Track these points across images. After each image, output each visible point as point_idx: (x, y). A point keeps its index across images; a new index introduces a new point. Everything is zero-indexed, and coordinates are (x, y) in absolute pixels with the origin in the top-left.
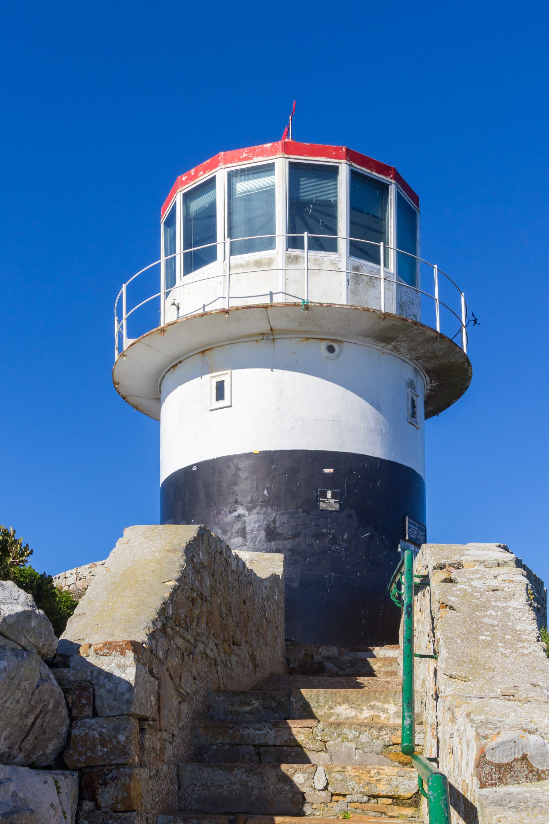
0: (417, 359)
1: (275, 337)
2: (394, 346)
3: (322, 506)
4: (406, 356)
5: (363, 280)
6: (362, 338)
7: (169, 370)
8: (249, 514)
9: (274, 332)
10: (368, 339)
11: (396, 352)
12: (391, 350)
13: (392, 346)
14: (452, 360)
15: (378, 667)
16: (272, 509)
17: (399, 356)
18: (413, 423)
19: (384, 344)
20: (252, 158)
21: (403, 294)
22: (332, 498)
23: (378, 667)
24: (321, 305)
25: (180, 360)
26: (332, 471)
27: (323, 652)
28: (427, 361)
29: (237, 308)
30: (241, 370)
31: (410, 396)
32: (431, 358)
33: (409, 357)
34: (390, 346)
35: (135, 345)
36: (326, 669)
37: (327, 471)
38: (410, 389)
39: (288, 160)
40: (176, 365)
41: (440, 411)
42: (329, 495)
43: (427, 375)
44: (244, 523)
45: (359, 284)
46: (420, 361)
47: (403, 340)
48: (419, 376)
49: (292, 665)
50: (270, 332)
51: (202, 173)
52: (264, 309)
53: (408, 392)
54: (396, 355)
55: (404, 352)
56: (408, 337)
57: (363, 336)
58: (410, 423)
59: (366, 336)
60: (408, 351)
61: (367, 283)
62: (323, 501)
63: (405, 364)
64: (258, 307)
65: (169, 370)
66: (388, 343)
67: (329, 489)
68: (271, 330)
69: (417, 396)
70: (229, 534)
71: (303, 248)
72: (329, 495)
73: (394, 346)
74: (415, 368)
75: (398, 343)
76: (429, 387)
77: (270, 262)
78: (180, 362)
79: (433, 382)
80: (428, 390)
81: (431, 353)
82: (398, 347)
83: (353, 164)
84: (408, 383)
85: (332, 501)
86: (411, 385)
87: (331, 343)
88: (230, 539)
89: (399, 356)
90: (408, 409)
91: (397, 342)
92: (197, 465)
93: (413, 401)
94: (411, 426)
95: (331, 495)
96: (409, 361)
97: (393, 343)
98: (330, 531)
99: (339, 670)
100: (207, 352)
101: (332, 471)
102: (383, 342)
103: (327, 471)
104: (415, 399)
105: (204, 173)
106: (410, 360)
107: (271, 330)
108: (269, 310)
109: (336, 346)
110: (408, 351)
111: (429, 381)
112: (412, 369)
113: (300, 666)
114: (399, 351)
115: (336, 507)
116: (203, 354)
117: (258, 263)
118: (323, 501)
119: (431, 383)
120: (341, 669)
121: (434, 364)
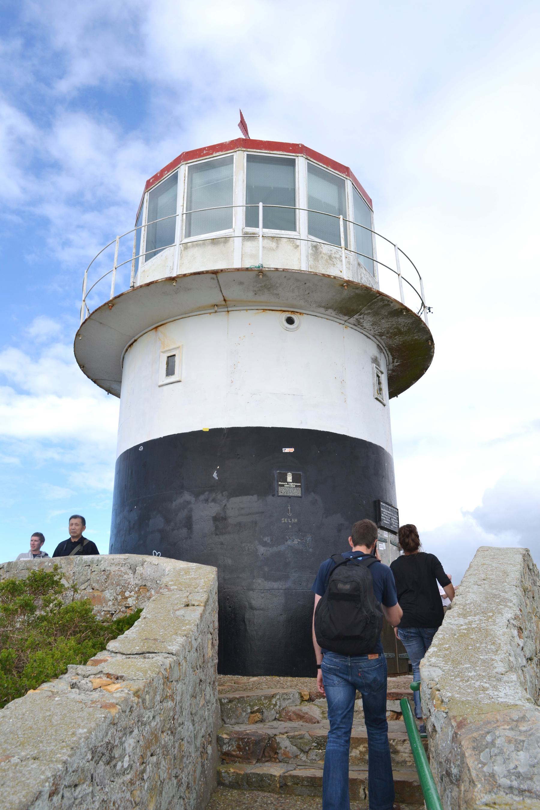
0: (381, 335)
1: (230, 309)
2: (357, 319)
3: (282, 491)
4: (370, 332)
5: (322, 257)
6: (322, 310)
7: (127, 350)
8: (196, 500)
9: (228, 302)
10: (330, 311)
11: (359, 326)
12: (354, 325)
13: (355, 319)
14: (416, 337)
15: (361, 752)
16: (223, 495)
17: (362, 331)
18: (380, 399)
19: (346, 318)
20: (212, 154)
21: (363, 275)
22: (293, 482)
23: (361, 752)
24: (277, 269)
25: (135, 338)
26: (292, 450)
27: (278, 704)
28: (390, 337)
29: (185, 275)
30: (330, 431)
31: (375, 372)
32: (395, 334)
33: (372, 332)
34: (352, 320)
35: (87, 322)
36: (280, 748)
37: (287, 450)
38: (375, 365)
39: (246, 153)
40: (132, 344)
41: (399, 393)
42: (289, 478)
43: (389, 354)
44: (191, 510)
45: (318, 261)
46: (383, 337)
47: (366, 312)
48: (382, 354)
49: (225, 748)
50: (223, 303)
51: (166, 172)
52: (214, 276)
53: (373, 368)
54: (359, 330)
55: (367, 327)
56: (372, 309)
57: (324, 307)
58: (377, 399)
59: (327, 308)
60: (371, 325)
61: (326, 261)
62: (283, 485)
63: (368, 339)
64: (207, 272)
65: (127, 350)
66: (351, 316)
67: (290, 471)
68: (225, 300)
69: (382, 373)
70: (172, 524)
71: (257, 226)
72: (289, 478)
73: (357, 319)
74: (378, 345)
75: (362, 317)
76: (391, 367)
77: (226, 239)
78: (135, 341)
79: (395, 361)
80: (390, 370)
81: (395, 328)
82: (362, 321)
83: (309, 158)
84: (372, 359)
85: (293, 485)
86: (375, 360)
87: (289, 315)
88: (173, 530)
89: (362, 331)
90: (374, 384)
91: (360, 315)
92: (144, 444)
93: (378, 376)
94: (378, 402)
95: (291, 478)
96: (373, 339)
97: (356, 317)
98: (291, 520)
99: (299, 753)
100: (160, 328)
101: (292, 450)
102: (345, 315)
103: (287, 450)
104: (380, 375)
105: (168, 172)
106: (374, 336)
107: (225, 300)
108: (220, 276)
109: (294, 316)
110: (371, 325)
111: (391, 360)
112: (375, 346)
113: (239, 748)
114: (362, 326)
115: (297, 492)
116: (156, 331)
117: (214, 241)
118: (283, 485)
119: (393, 362)
120: (302, 751)
121: (397, 340)
